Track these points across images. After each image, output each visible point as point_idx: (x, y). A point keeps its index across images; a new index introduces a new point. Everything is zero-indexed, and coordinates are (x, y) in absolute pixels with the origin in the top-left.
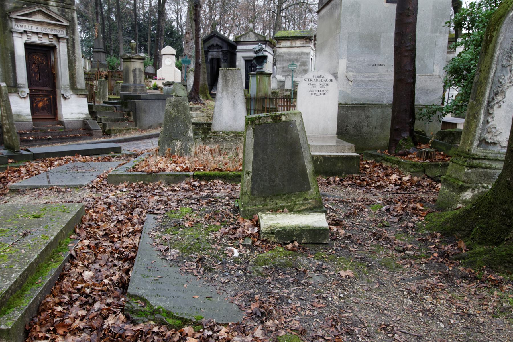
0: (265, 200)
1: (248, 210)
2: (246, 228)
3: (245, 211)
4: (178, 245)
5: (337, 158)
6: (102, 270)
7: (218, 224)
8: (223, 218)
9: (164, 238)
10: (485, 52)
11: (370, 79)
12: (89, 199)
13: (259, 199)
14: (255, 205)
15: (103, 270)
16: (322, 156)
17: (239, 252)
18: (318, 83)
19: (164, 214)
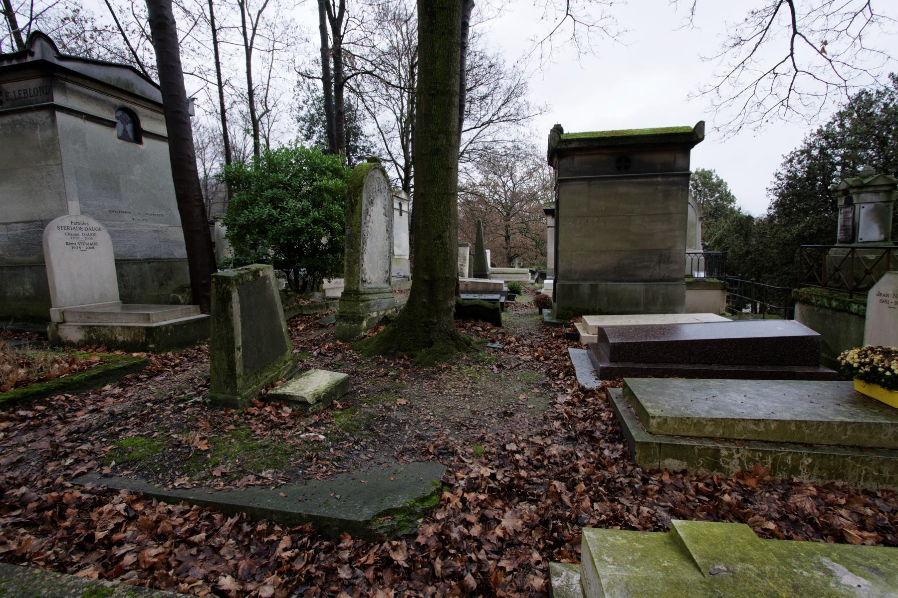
5: (188, 323)
10: (352, 212)
11: (116, 229)
16: (171, 324)
18: (80, 232)
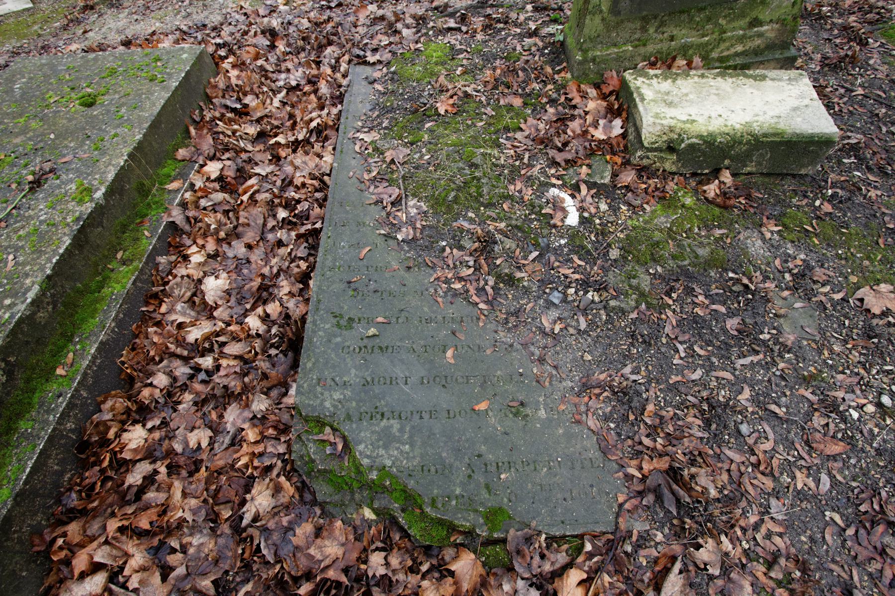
0: (644, 29)
1: (594, 60)
2: (589, 119)
3: (585, 61)
4: (424, 185)
6: (253, 258)
7: (517, 102)
8: (527, 82)
9: (389, 156)
12: (237, 17)
13: (630, 25)
14: (615, 45)
15: (256, 256)
17: (581, 209)
19: (388, 64)
